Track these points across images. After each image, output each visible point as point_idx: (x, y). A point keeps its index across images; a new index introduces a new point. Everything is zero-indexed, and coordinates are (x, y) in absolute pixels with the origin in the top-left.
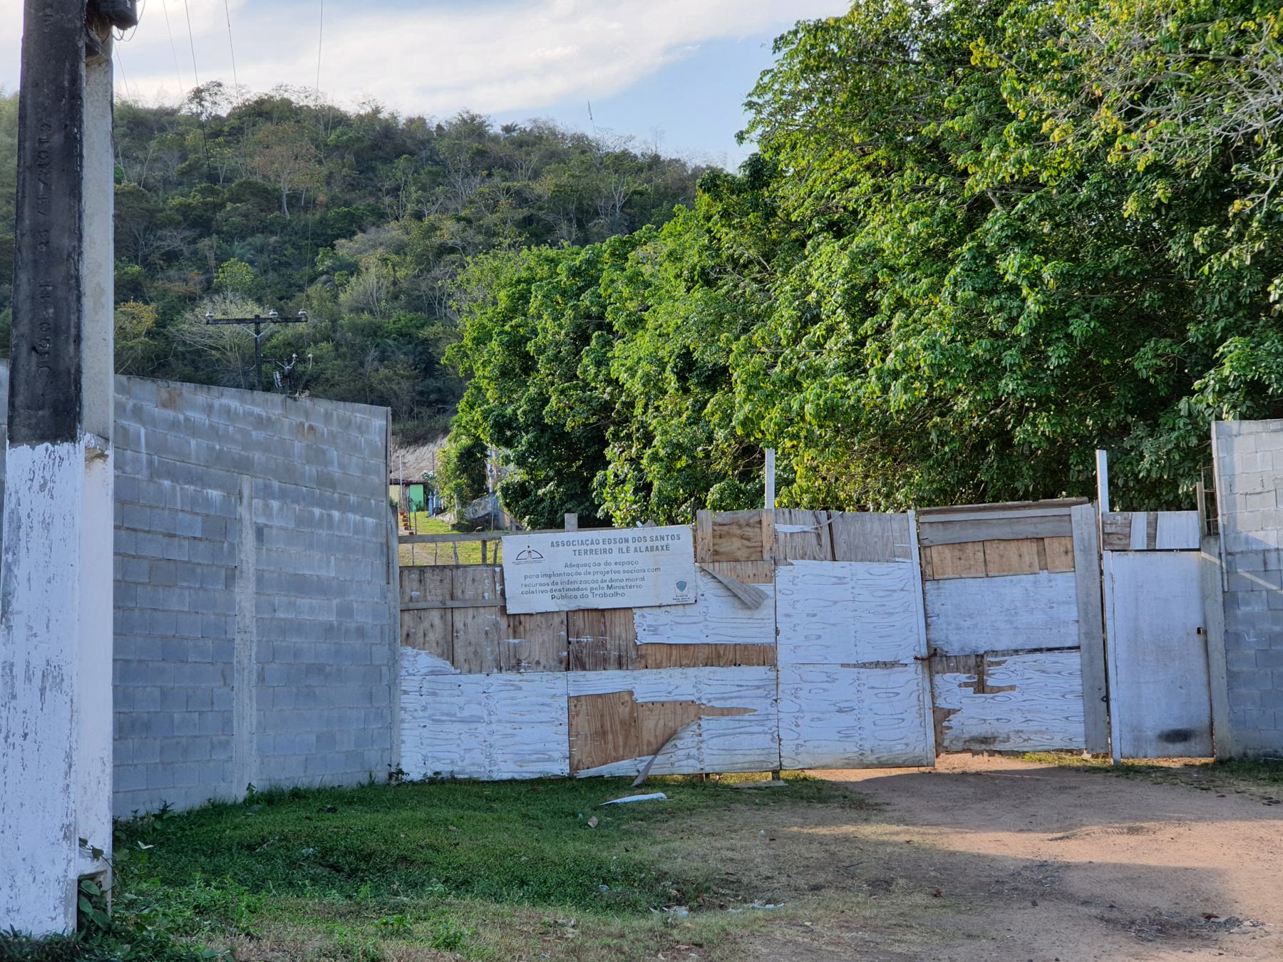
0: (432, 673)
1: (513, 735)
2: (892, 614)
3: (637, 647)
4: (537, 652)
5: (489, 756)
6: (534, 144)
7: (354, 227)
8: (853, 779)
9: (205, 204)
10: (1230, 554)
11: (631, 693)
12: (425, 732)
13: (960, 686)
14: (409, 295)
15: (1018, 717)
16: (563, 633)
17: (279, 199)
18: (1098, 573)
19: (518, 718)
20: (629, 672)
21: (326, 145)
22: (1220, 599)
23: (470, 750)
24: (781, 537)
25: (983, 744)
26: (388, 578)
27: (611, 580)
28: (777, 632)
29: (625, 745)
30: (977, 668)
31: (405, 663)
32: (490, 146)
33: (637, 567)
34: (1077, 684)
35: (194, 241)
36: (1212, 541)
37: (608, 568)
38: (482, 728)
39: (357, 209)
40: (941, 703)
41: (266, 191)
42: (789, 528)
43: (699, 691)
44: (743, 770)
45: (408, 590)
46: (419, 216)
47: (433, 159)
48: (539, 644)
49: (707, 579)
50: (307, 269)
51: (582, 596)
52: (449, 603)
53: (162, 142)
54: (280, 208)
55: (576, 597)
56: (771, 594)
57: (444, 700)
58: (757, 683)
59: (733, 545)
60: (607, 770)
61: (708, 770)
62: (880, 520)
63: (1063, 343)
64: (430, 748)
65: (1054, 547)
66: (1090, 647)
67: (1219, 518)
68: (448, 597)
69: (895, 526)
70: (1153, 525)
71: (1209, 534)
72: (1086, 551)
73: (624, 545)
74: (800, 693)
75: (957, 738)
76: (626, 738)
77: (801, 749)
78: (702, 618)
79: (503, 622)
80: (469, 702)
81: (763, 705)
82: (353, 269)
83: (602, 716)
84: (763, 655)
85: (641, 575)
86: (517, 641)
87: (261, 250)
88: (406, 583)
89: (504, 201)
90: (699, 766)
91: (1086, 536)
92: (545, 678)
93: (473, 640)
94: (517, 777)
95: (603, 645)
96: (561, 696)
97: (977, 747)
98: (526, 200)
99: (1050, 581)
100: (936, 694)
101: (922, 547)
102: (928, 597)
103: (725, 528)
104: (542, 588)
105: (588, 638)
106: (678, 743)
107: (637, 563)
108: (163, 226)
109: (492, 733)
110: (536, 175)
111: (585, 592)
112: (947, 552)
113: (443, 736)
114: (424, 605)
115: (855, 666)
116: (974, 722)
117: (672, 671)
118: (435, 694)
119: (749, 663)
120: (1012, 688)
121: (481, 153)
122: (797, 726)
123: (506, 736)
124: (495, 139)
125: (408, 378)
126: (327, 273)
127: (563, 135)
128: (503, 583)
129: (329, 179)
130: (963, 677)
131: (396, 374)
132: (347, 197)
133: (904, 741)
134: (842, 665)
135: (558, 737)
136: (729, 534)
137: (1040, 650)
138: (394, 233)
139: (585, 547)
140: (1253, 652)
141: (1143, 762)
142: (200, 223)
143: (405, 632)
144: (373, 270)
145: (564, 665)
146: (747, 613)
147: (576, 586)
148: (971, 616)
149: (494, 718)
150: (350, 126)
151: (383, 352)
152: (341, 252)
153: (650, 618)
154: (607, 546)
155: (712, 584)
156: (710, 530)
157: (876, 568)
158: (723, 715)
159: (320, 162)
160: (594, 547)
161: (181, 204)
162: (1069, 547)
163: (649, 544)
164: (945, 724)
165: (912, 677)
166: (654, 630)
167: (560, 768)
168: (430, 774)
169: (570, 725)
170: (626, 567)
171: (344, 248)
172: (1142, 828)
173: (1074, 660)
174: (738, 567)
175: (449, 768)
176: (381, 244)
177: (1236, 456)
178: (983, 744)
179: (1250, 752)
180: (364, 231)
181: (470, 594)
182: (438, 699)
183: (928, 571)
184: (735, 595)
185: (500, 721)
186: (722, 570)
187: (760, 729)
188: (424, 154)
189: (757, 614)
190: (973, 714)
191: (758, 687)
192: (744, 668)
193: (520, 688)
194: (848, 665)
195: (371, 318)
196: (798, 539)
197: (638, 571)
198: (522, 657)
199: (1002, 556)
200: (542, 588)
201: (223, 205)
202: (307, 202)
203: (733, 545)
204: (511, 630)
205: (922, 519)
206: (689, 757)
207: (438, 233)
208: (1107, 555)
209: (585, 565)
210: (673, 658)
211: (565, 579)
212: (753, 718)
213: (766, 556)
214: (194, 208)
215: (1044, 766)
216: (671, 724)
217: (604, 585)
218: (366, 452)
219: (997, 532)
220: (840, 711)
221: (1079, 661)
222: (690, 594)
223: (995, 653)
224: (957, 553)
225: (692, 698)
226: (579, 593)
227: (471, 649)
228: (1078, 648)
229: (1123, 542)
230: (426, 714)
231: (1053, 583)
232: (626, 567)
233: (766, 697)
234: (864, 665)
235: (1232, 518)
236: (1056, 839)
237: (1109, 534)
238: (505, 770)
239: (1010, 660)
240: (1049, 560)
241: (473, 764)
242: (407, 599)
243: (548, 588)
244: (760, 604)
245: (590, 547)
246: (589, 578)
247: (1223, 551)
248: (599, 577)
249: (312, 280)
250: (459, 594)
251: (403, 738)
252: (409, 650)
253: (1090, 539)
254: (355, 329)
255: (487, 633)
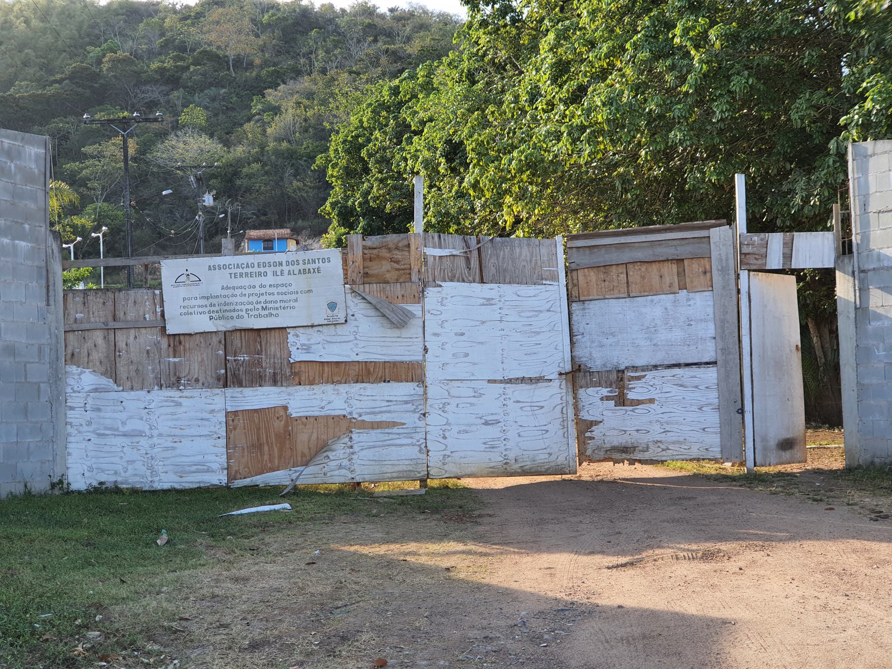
0: (96, 390)
1: (173, 448)
2: (538, 333)
3: (291, 365)
4: (196, 370)
5: (151, 468)
6: (409, 19)
7: (279, 81)
8: (473, 486)
9: (176, 67)
10: (863, 271)
11: (285, 408)
12: (90, 446)
13: (602, 399)
14: (316, 129)
15: (657, 428)
16: (221, 352)
17: (228, 63)
18: (735, 292)
19: (177, 432)
20: (283, 389)
21: (262, 24)
22: (852, 315)
23: (133, 462)
24: (430, 261)
25: (623, 452)
26: (48, 300)
27: (266, 302)
28: (426, 350)
29: (280, 457)
30: (618, 383)
31: (70, 381)
32: (377, 21)
33: (291, 289)
34: (713, 397)
35: (167, 94)
36: (846, 261)
37: (263, 290)
38: (144, 442)
39: (281, 68)
40: (585, 415)
41: (218, 56)
42: (438, 252)
43: (351, 406)
44: (391, 479)
45: (72, 312)
46: (324, 71)
47: (337, 31)
48: (195, 362)
49: (358, 300)
50: (245, 112)
51: (238, 317)
52: (112, 324)
53: (148, 24)
54: (229, 69)
55: (232, 318)
56: (419, 313)
57: (108, 415)
58: (405, 398)
59: (383, 268)
60: (260, 480)
61: (358, 479)
62: (528, 245)
63: (727, 98)
64: (94, 460)
65: (693, 268)
66: (726, 362)
67: (853, 238)
68: (110, 318)
69: (544, 251)
70: (789, 246)
71: (844, 253)
72: (723, 270)
73: (278, 269)
74: (447, 408)
75: (599, 448)
76: (281, 450)
77: (447, 460)
78: (352, 338)
79: (164, 342)
80: (130, 417)
81: (411, 419)
82: (276, 110)
83: (258, 429)
84: (411, 372)
85: (294, 296)
86: (177, 360)
87: (213, 99)
88: (70, 305)
89: (384, 60)
90: (350, 476)
91: (724, 258)
92: (204, 394)
93: (135, 359)
94: (177, 486)
95: (259, 363)
96: (219, 411)
97: (617, 456)
98: (400, 58)
99: (688, 300)
100: (580, 406)
101: (568, 271)
102: (574, 318)
103: (375, 251)
104: (201, 310)
105: (245, 355)
106: (330, 454)
107: (290, 285)
108: (146, 83)
109: (153, 446)
110: (409, 39)
111: (240, 313)
112: (592, 275)
113: (107, 449)
114: (87, 326)
115: (501, 382)
116: (616, 433)
117: (323, 387)
118: (99, 410)
119: (398, 380)
120: (651, 401)
121: (370, 26)
122: (445, 438)
123: (167, 449)
124: (382, 17)
125: (313, 188)
126: (259, 114)
127: (432, 13)
128: (162, 306)
129: (262, 49)
130: (605, 391)
131: (305, 185)
132: (276, 60)
133: (548, 451)
134: (489, 381)
135: (215, 450)
136: (379, 258)
137: (678, 365)
138: (306, 84)
139: (240, 270)
140: (882, 365)
141: (772, 470)
142: (171, 80)
143: (69, 351)
144: (290, 111)
145: (221, 383)
146: (396, 333)
147: (232, 308)
148: (613, 334)
149: (155, 432)
150: (279, 10)
151: (297, 170)
152: (269, 98)
153: (303, 337)
154: (262, 270)
155: (363, 305)
156: (361, 254)
157: (531, 290)
158: (373, 428)
159: (257, 36)
160: (249, 270)
161: (159, 68)
162: (708, 267)
163: (301, 267)
164: (588, 434)
165: (554, 393)
166: (307, 349)
167: (219, 478)
168: (95, 484)
169: (228, 438)
170: (280, 289)
171: (272, 96)
172: (719, 551)
173: (711, 375)
174: (386, 286)
175: (112, 479)
176: (297, 92)
177: (871, 178)
178: (623, 452)
179: (877, 460)
180: (285, 83)
181: (131, 316)
182: (102, 414)
183: (575, 293)
184: (384, 316)
185: (160, 435)
186: (372, 290)
187: (409, 441)
188: (330, 28)
189: (405, 333)
190: (613, 424)
191: (406, 402)
192: (394, 385)
193: (180, 404)
194: (495, 381)
195: (289, 146)
196: (447, 263)
197: (291, 293)
198: (181, 375)
199: (643, 278)
200: (201, 310)
201: (188, 68)
202: (248, 64)
203: (383, 268)
204: (171, 349)
205: (570, 244)
206: (340, 467)
207: (336, 83)
208: (744, 275)
209: (241, 287)
210: (325, 375)
211: (222, 300)
212: (401, 431)
213: (414, 277)
214: (168, 70)
215: (684, 473)
216: (324, 437)
217: (259, 306)
218: (18, 177)
219: (639, 255)
220: (486, 423)
221: (715, 375)
222: (341, 315)
223: (635, 368)
224: (602, 276)
225: (344, 413)
226: (235, 314)
227: (133, 368)
228: (715, 363)
229: (760, 262)
230: (91, 429)
231: (692, 302)
232: (280, 289)
233: (414, 411)
234: (510, 381)
235: (866, 237)
236: (617, 566)
237: (746, 254)
238: (166, 480)
239: (650, 375)
240: (688, 280)
241: (136, 475)
242: (72, 320)
243: (206, 310)
244: (406, 323)
245: (246, 270)
246: (245, 299)
247: (856, 269)
248: (254, 299)
249: (249, 120)
250: (122, 315)
251: (70, 451)
252: (73, 369)
253: (727, 260)
254: (276, 152)
255: (148, 352)
